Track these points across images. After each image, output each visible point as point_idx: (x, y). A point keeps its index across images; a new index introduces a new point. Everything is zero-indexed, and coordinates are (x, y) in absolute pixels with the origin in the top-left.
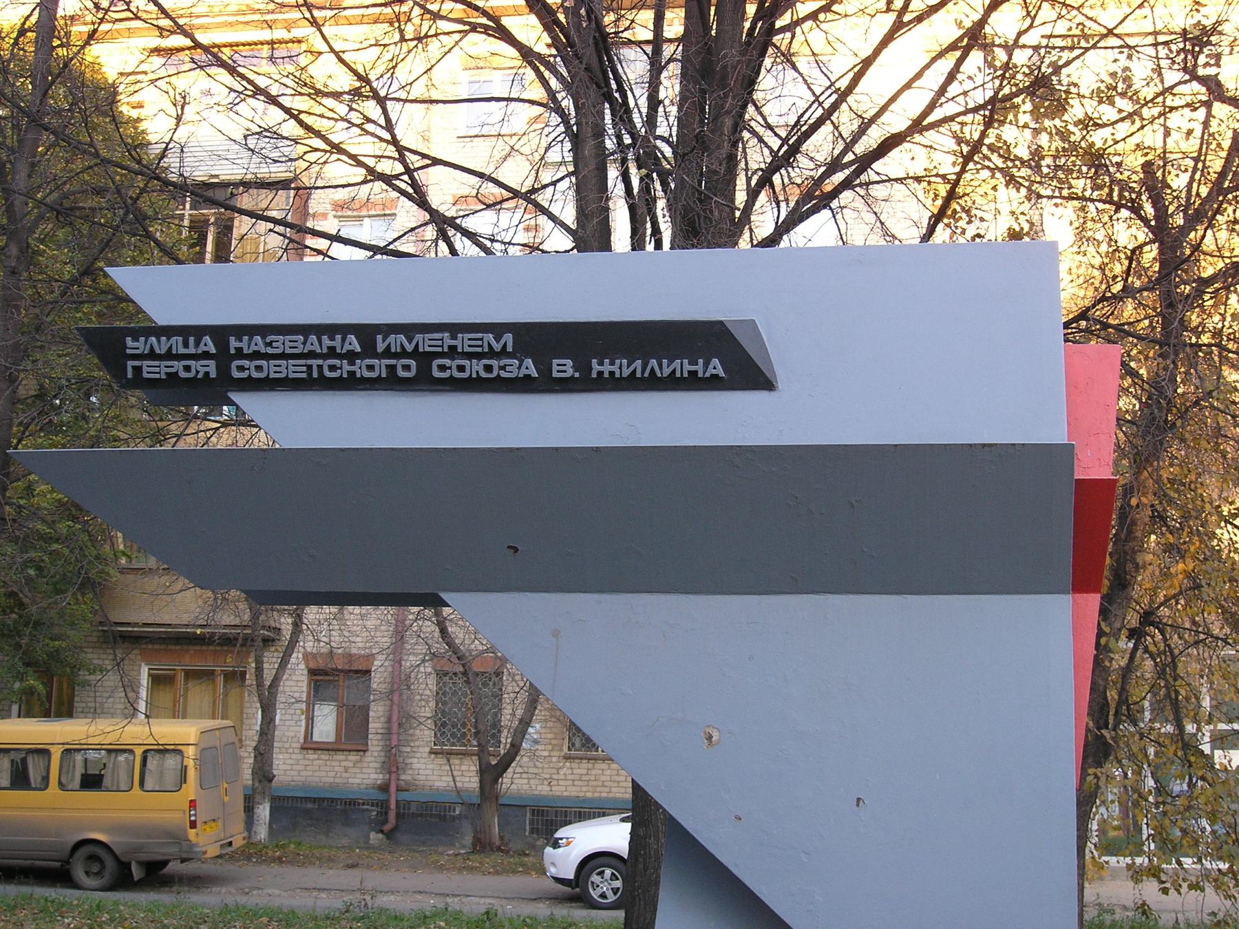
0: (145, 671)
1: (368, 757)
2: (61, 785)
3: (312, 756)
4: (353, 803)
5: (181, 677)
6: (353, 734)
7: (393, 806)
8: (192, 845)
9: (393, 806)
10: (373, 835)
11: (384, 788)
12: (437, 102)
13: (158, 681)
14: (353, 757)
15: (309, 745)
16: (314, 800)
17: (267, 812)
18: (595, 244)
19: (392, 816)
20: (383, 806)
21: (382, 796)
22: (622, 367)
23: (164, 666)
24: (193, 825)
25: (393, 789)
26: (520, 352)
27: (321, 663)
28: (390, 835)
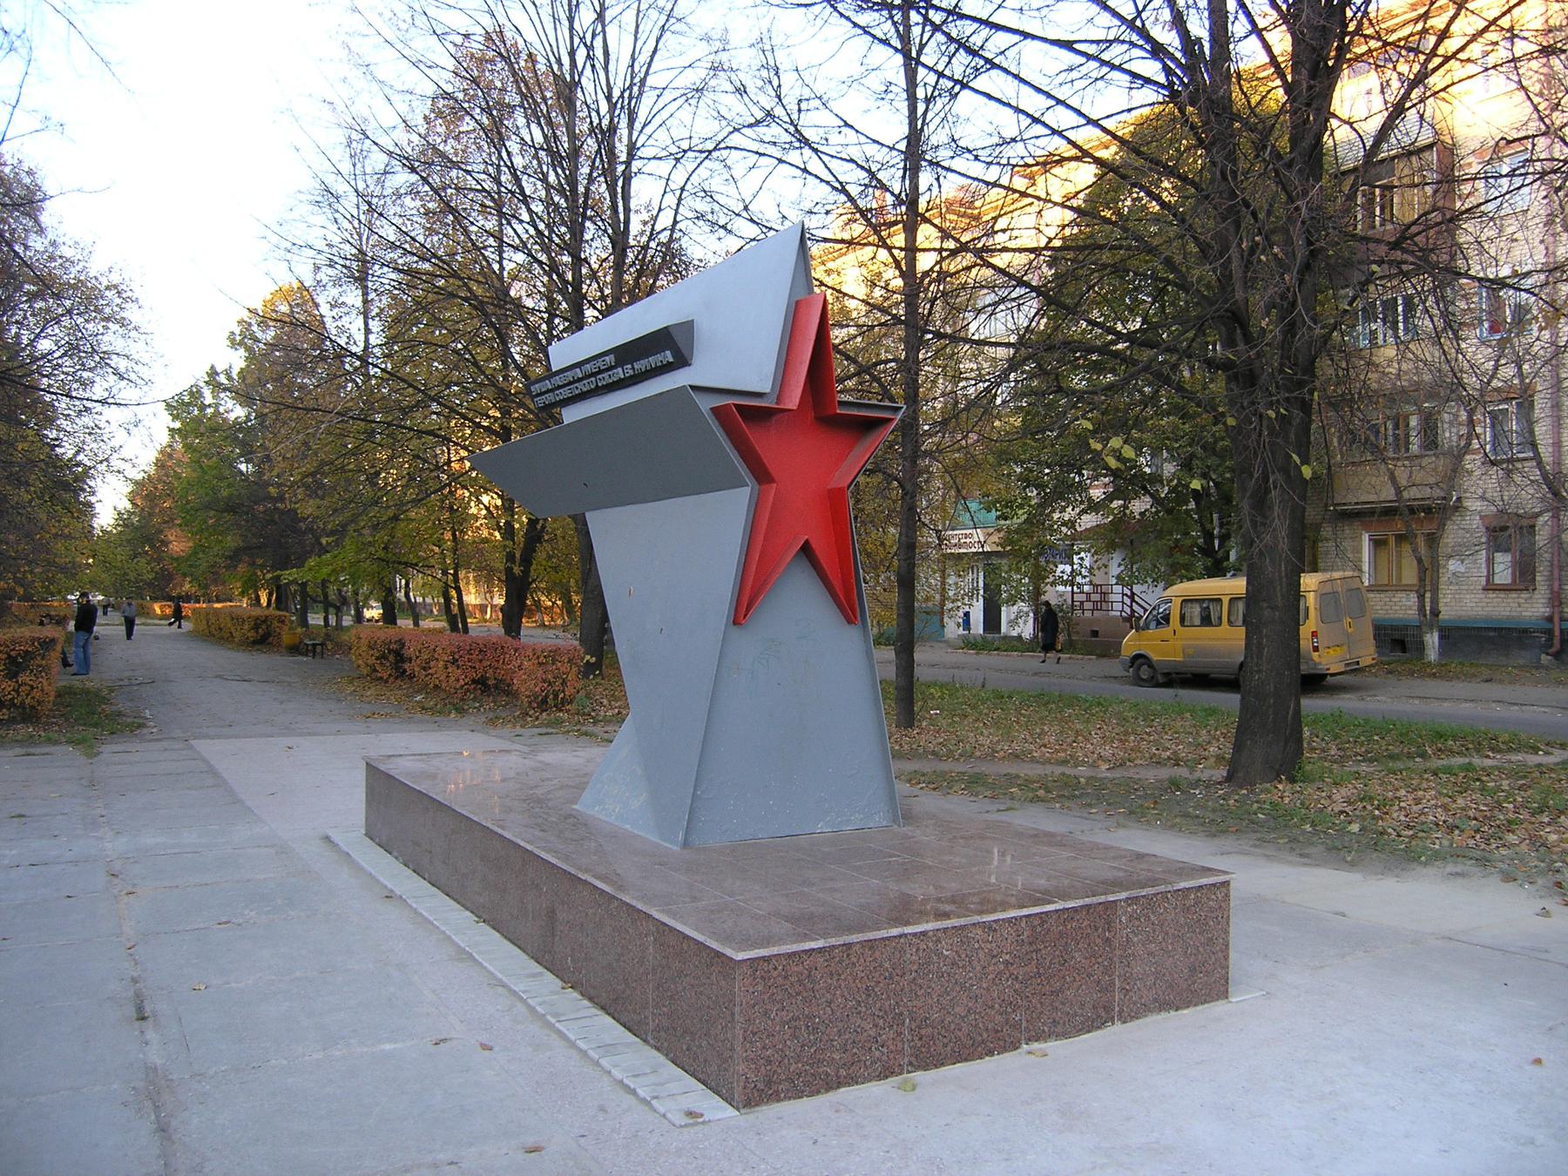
0: (1366, 537)
1: (1537, 595)
2: (1230, 623)
3: (1491, 595)
4: (1525, 631)
5: (1392, 541)
6: (1525, 576)
7: (1557, 633)
8: (1316, 664)
9: (1557, 633)
10: (1543, 656)
11: (1550, 619)
12: (1034, 37)
13: (1378, 544)
14: (1525, 595)
15: (1490, 587)
16: (1495, 629)
17: (1436, 639)
18: (1327, 83)
19: (1557, 642)
20: (1549, 632)
21: (1548, 626)
22: (600, 363)
23: (1379, 535)
24: (1316, 649)
25: (1556, 619)
26: (620, 363)
27: (1495, 524)
28: (1557, 655)
